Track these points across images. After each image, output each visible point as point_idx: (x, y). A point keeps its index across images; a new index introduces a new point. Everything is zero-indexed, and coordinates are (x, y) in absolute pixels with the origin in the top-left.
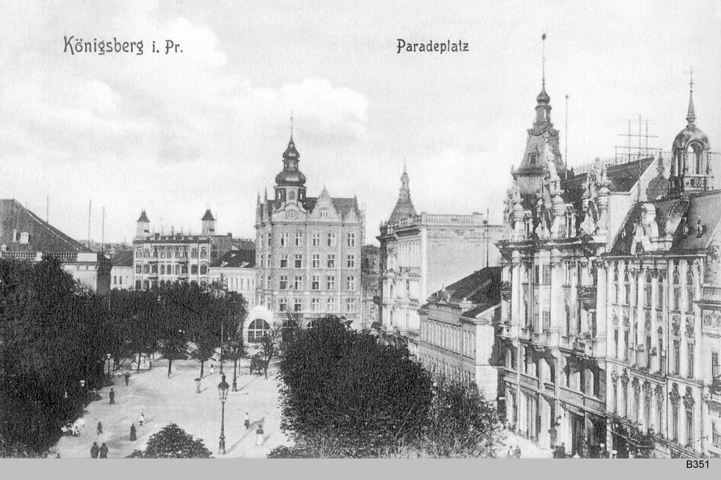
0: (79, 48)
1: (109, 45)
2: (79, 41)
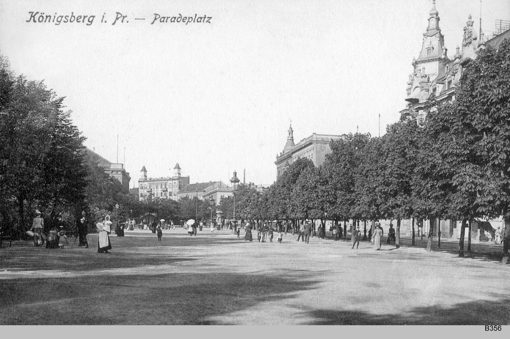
1: (67, 18)
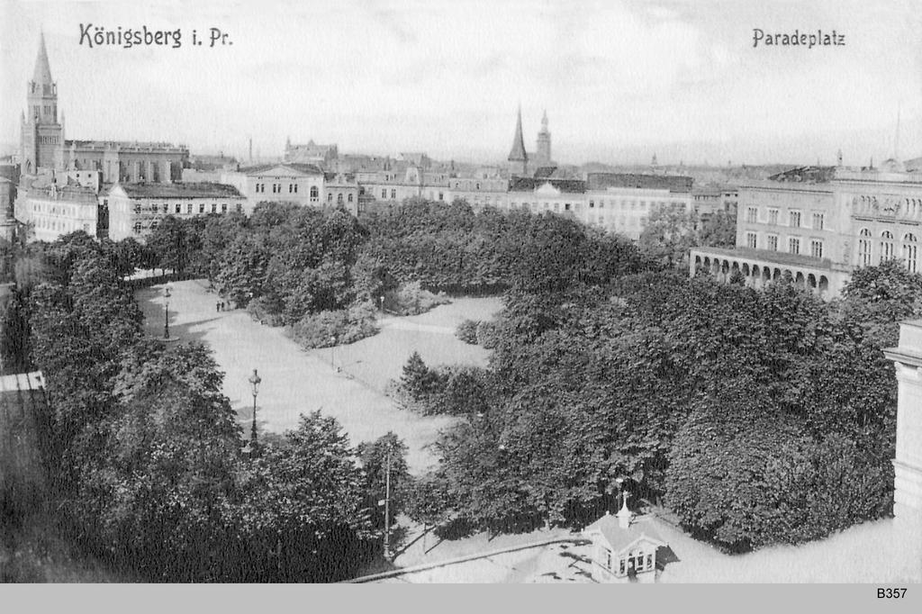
0: (99, 39)
1: (137, 35)
2: (100, 31)
